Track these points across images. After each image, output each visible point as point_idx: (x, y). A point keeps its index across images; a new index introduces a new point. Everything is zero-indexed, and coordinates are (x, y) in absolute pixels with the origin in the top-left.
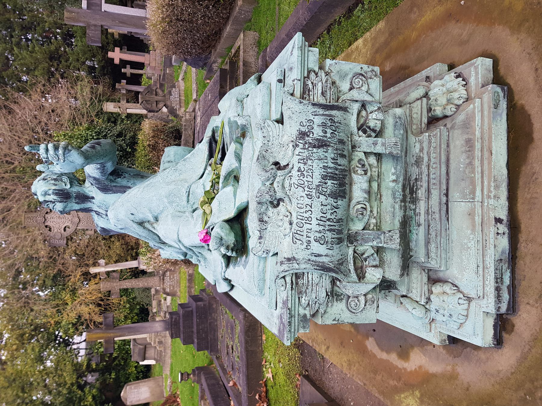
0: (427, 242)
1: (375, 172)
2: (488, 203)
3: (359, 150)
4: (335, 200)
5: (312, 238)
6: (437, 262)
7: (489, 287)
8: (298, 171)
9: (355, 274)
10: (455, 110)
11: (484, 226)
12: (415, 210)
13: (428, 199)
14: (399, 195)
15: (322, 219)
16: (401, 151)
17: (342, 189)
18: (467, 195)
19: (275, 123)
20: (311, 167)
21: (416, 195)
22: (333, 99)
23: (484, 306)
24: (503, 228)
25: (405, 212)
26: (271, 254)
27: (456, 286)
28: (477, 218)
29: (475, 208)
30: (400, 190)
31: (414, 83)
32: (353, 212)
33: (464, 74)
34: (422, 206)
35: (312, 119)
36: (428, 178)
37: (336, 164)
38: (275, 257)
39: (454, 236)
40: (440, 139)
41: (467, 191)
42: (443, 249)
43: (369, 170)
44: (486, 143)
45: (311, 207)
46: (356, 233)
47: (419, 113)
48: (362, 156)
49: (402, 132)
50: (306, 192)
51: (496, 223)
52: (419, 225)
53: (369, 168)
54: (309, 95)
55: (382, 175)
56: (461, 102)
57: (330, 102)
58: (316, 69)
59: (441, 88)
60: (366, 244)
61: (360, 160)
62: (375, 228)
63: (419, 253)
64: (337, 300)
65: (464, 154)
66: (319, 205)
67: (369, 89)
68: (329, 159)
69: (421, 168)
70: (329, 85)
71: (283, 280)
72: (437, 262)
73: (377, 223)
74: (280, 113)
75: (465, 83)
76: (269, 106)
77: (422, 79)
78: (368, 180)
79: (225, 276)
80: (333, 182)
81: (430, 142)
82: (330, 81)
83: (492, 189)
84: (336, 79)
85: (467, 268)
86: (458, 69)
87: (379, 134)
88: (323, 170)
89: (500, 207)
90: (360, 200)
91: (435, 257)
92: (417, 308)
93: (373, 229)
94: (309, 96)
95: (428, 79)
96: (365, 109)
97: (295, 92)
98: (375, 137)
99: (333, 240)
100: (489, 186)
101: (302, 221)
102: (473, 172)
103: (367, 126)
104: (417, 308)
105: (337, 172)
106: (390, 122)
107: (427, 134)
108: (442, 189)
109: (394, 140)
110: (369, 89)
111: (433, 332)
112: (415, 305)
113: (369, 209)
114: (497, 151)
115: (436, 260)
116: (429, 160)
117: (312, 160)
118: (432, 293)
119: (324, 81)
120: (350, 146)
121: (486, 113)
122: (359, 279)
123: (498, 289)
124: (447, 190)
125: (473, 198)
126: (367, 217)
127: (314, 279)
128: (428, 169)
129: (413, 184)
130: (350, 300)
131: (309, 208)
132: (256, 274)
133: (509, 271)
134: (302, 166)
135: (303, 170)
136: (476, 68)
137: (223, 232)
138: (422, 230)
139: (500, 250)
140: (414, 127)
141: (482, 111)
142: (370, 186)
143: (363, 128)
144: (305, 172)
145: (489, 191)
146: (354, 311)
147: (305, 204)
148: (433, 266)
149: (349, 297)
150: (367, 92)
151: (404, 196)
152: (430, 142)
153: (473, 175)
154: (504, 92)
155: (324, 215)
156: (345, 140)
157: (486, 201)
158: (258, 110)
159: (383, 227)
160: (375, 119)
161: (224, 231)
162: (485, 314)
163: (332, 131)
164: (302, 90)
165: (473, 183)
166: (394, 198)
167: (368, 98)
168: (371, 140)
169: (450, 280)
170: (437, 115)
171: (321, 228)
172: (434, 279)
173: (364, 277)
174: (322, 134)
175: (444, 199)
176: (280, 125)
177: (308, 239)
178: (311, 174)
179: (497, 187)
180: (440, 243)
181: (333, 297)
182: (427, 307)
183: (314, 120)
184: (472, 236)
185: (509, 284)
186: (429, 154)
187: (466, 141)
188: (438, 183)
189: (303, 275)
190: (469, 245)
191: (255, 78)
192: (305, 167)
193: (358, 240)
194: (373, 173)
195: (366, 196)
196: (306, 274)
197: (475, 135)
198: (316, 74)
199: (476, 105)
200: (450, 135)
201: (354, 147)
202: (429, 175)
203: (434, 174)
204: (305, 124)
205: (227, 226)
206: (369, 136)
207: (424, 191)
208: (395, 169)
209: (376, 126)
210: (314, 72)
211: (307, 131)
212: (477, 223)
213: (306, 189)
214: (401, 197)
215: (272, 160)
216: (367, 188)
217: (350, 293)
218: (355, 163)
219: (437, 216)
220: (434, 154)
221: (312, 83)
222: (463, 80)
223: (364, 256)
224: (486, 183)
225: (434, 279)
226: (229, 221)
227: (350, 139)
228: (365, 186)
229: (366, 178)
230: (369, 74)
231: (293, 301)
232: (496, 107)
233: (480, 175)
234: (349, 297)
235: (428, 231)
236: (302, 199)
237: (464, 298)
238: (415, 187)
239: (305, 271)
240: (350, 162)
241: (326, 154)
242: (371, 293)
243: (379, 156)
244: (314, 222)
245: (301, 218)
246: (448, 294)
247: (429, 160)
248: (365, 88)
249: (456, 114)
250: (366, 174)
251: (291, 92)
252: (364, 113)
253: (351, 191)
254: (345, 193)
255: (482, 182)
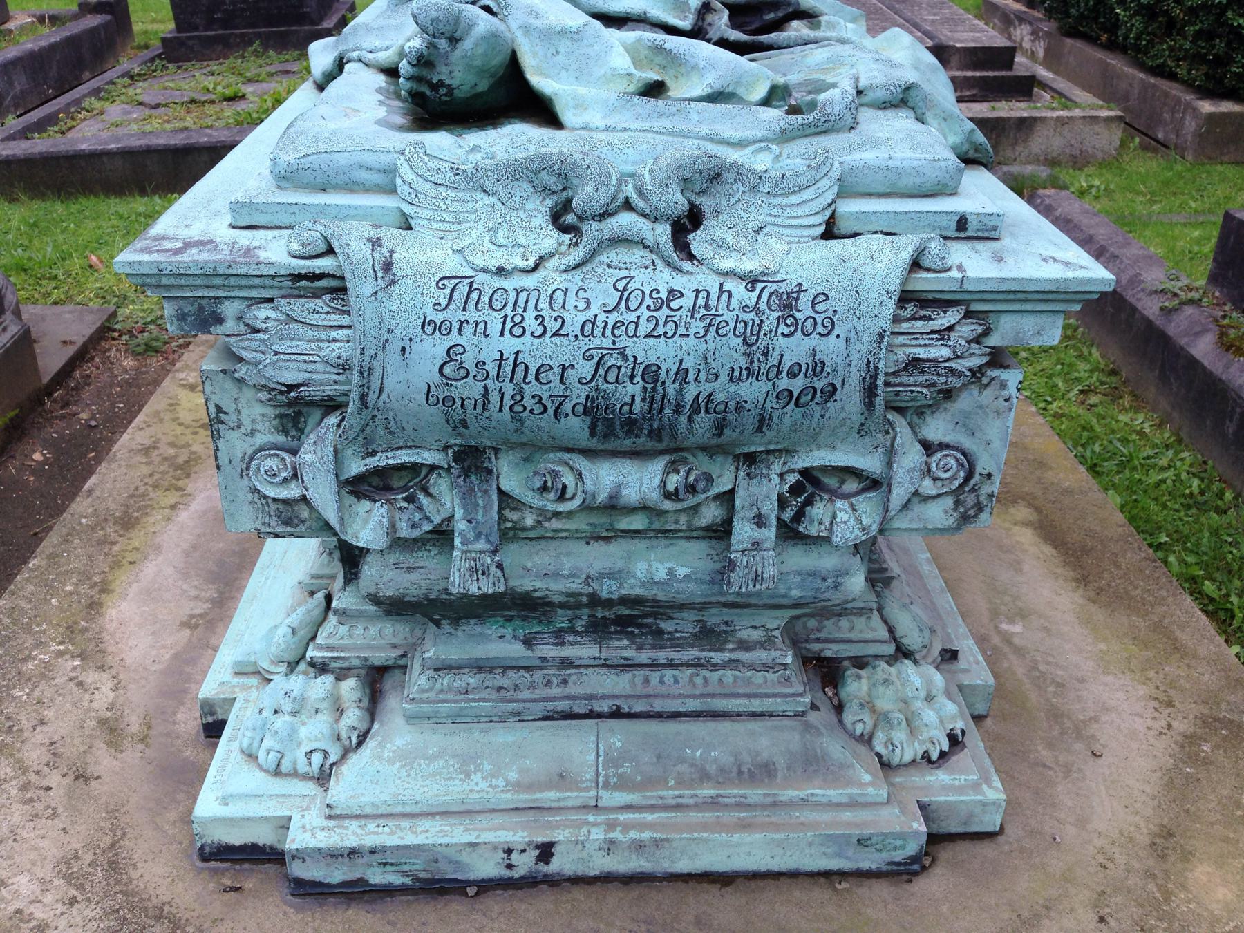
0: (481, 663)
1: (677, 522)
2: (595, 824)
3: (741, 474)
4: (580, 409)
5: (459, 340)
6: (424, 691)
7: (360, 831)
8: (671, 291)
9: (363, 469)
10: (858, 732)
11: (531, 813)
12: (572, 630)
13: (604, 666)
14: (607, 589)
15: (520, 370)
16: (739, 594)
17: (618, 427)
18: (617, 767)
19: (828, 213)
20: (681, 330)
21: (616, 632)
22: (897, 394)
23: (306, 820)
24: (525, 863)
25: (562, 605)
26: (407, 209)
27: (360, 744)
28: (552, 795)
29: (580, 790)
30: (623, 592)
31: (940, 617)
32: (549, 462)
33: (962, 755)
34: (586, 651)
35: (836, 332)
36: (664, 665)
37: (695, 408)
38: (398, 220)
39: (504, 736)
40: (775, 696)
41: (626, 768)
42: (462, 708)
43: (679, 506)
44: (760, 817)
45: (556, 334)
46: (490, 472)
47: (852, 636)
48: (723, 485)
49: (795, 593)
50: (602, 317)
51: (538, 847)
52: (528, 642)
53: (685, 505)
54: (913, 318)
55: (668, 542)
56: (879, 748)
57: (887, 384)
58: (994, 340)
59: (923, 694)
60: (457, 500)
61: (709, 479)
62: (509, 525)
63: (440, 646)
64: (281, 416)
65: (732, 759)
66: (563, 360)
67: (926, 499)
68: (709, 387)
69: (692, 646)
70: (943, 379)
71: (323, 247)
72: (424, 691)
73: (524, 529)
74: (857, 229)
75: (934, 757)
76: (882, 190)
77: (951, 641)
78: (649, 504)
79: (349, 61)
80: (638, 399)
81: (766, 667)
82: (953, 382)
83: (633, 835)
84: (965, 401)
85: (413, 773)
86: (975, 741)
87: (790, 533)
88: (674, 369)
89: (584, 854)
90: (588, 481)
91: (438, 686)
92: (296, 638)
93: (506, 520)
94: (909, 320)
95: (950, 655)
96: (864, 490)
97: (924, 275)
98: (778, 519)
99: (459, 402)
100: (642, 826)
101: (509, 308)
102: (680, 783)
103: (812, 495)
104: (296, 638)
105: (667, 410)
106: (826, 561)
107: (789, 660)
108: (631, 702)
109: (771, 571)
110: (926, 499)
111: (236, 680)
112: (304, 633)
113: (562, 507)
114: (738, 845)
115: (431, 689)
116: (716, 667)
117: (706, 333)
118: (338, 679)
119: (952, 364)
120: (753, 449)
121: (847, 815)
122: (348, 482)
123: (353, 853)
124: (631, 716)
125: (606, 785)
126: (537, 502)
127: (333, 346)
128: (688, 665)
129: (647, 626)
130: (285, 455)
131: (553, 326)
132: (343, 160)
133: (408, 880)
134: (687, 302)
135: (674, 305)
136: (976, 787)
137: (477, 44)
138: (516, 650)
139: (465, 857)
140: (812, 623)
141: (853, 804)
142: (631, 510)
143: (810, 483)
144: (665, 311)
145: (627, 827)
146: (253, 467)
147: (564, 314)
148: (413, 680)
149: (294, 452)
150: (916, 493)
151: (609, 603)
152: (766, 667)
153: (672, 783)
154: (905, 864)
155: (531, 377)
156: (770, 434)
157: (601, 818)
158: (869, 156)
159: (514, 547)
160: (834, 517)
161: (480, 51)
162: (284, 822)
163: (796, 394)
164: (930, 297)
165: (649, 783)
166: (601, 576)
167: (899, 494)
168: (770, 508)
169: (376, 726)
170: (843, 686)
171: (492, 368)
172: (377, 680)
173: (359, 495)
174: (787, 363)
175: (604, 707)
176: (822, 229)
177: (456, 325)
178: (660, 331)
179: (639, 846)
180: (479, 700)
181: (289, 404)
182: (302, 666)
183: (833, 336)
184: (501, 783)
185: (372, 881)
186: (733, 664)
187: (766, 765)
188: (649, 690)
189: (344, 312)
190: (477, 778)
191: (977, 148)
192: (684, 312)
193: (467, 476)
194: (671, 517)
195: (602, 498)
196: (345, 320)
197: (785, 788)
198: (977, 340)
199: (870, 790)
200: (786, 722)
201: (750, 459)
202: (671, 665)
203: (676, 681)
204: (819, 308)
205: (499, 60)
206: (782, 503)
207: (625, 654)
208: (687, 578)
209: (812, 521)
210: (987, 332)
211: (798, 315)
212: (538, 796)
213: (613, 318)
214: (604, 595)
215: (705, 202)
216: (622, 502)
217: (307, 455)
218: (703, 464)
219: (555, 691)
220: (731, 680)
221: (950, 328)
222: (943, 755)
223: (421, 496)
224: (649, 817)
225: (377, 680)
226: (513, 65)
227: (772, 447)
228: (631, 495)
229: (654, 497)
230: (970, 499)
231: (257, 281)
232: (862, 842)
233: (673, 802)
234: (294, 452)
235: (513, 668)
236: (582, 305)
237: (327, 766)
238: (637, 631)
239: (355, 316)
240: (704, 449)
241: (724, 377)
242: (314, 516)
243: (721, 532)
244: (509, 345)
245: (521, 303)
246: (337, 721)
247: (715, 665)
248: (928, 487)
249: (845, 736)
250: (668, 496)
251: (926, 262)
252: (851, 485)
253: (614, 454)
254: (606, 436)
255: (652, 808)
